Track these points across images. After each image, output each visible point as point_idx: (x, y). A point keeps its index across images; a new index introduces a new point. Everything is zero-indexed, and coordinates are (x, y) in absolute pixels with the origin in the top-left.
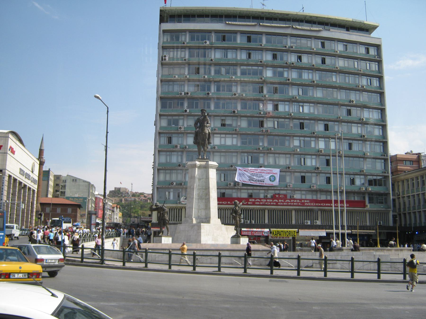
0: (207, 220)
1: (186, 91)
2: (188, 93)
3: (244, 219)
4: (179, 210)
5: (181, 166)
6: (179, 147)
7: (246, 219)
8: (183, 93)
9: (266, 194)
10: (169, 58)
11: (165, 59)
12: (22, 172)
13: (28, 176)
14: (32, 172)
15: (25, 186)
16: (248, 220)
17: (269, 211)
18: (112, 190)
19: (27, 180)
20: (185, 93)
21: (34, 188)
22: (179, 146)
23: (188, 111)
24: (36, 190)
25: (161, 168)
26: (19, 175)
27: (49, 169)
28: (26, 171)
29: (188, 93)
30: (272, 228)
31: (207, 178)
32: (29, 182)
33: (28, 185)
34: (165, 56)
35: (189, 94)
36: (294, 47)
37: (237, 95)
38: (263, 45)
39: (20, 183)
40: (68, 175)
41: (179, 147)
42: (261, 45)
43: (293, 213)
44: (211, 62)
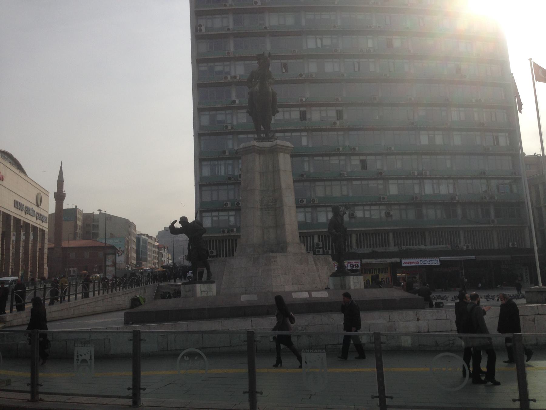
0: (281, 247)
1: (233, 74)
2: (235, 77)
3: (323, 248)
4: (232, 240)
5: (233, 179)
6: (227, 154)
7: (326, 249)
8: (229, 78)
9: (352, 212)
10: (206, 28)
11: (201, 30)
12: (17, 205)
13: (28, 211)
14: (38, 206)
15: (27, 225)
16: (329, 249)
17: (357, 235)
18: (161, 230)
19: (28, 216)
20: (231, 77)
21: (41, 228)
22: (227, 151)
23: (237, 102)
24: (46, 230)
25: (203, 183)
26: (13, 209)
27: (76, 207)
28: (26, 204)
29: (235, 77)
30: (364, 259)
31: (276, 170)
32: (34, 219)
33: (31, 223)
34: (200, 26)
35: (238, 78)
37: (304, 76)
38: (228, 5)
39: (17, 221)
40: (419, 345)
41: (227, 154)
42: (225, 5)
43: (391, 235)
44: (266, 31)
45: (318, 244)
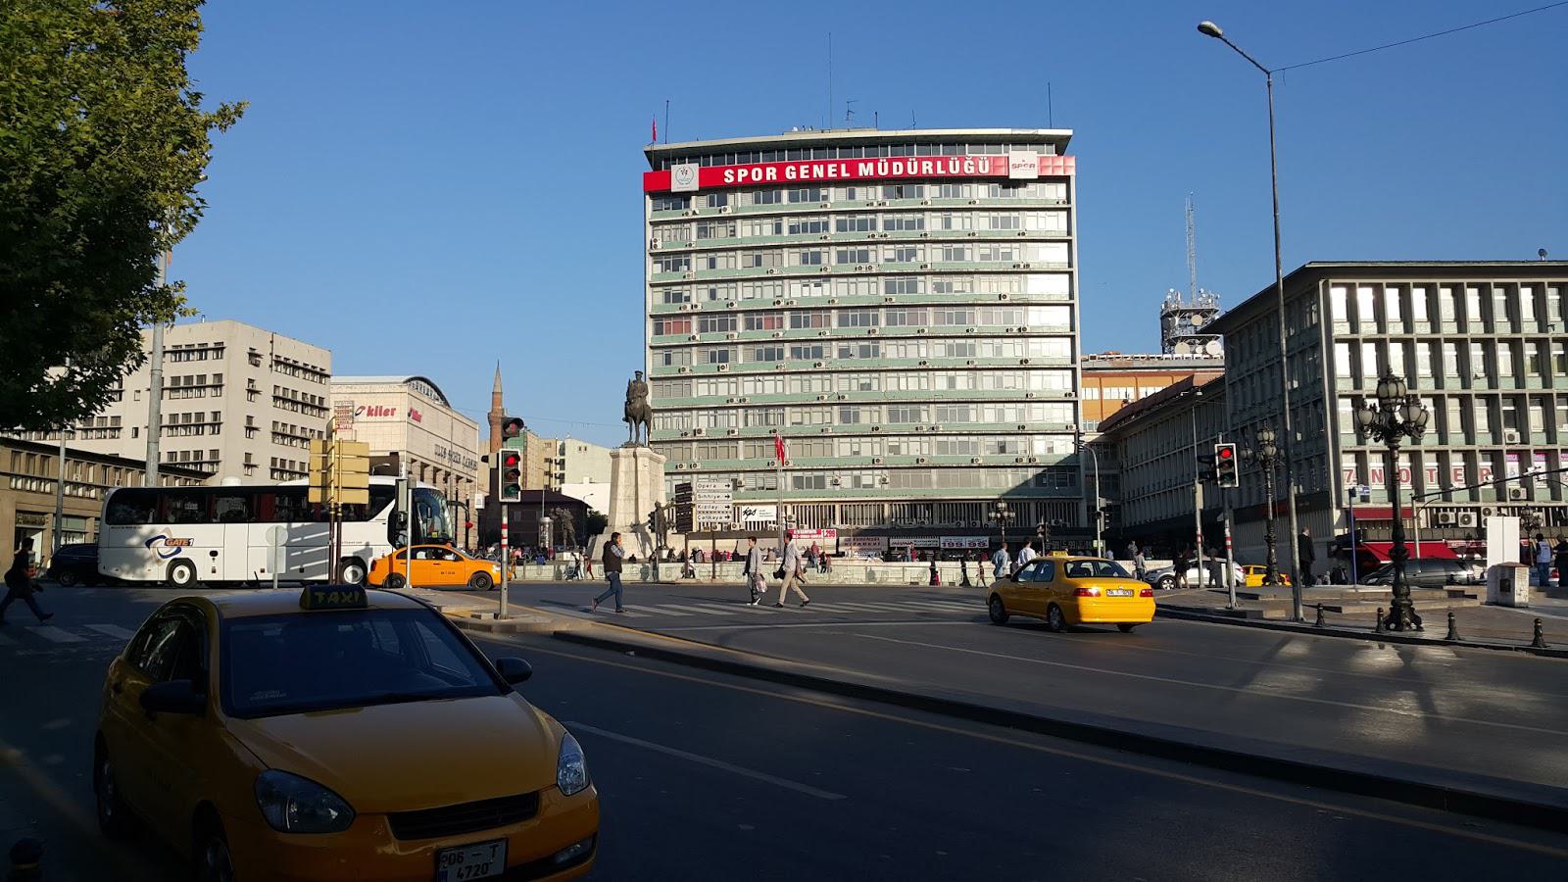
11: (656, 246)
34: (655, 240)
36: (888, 204)
45: (790, 517)
